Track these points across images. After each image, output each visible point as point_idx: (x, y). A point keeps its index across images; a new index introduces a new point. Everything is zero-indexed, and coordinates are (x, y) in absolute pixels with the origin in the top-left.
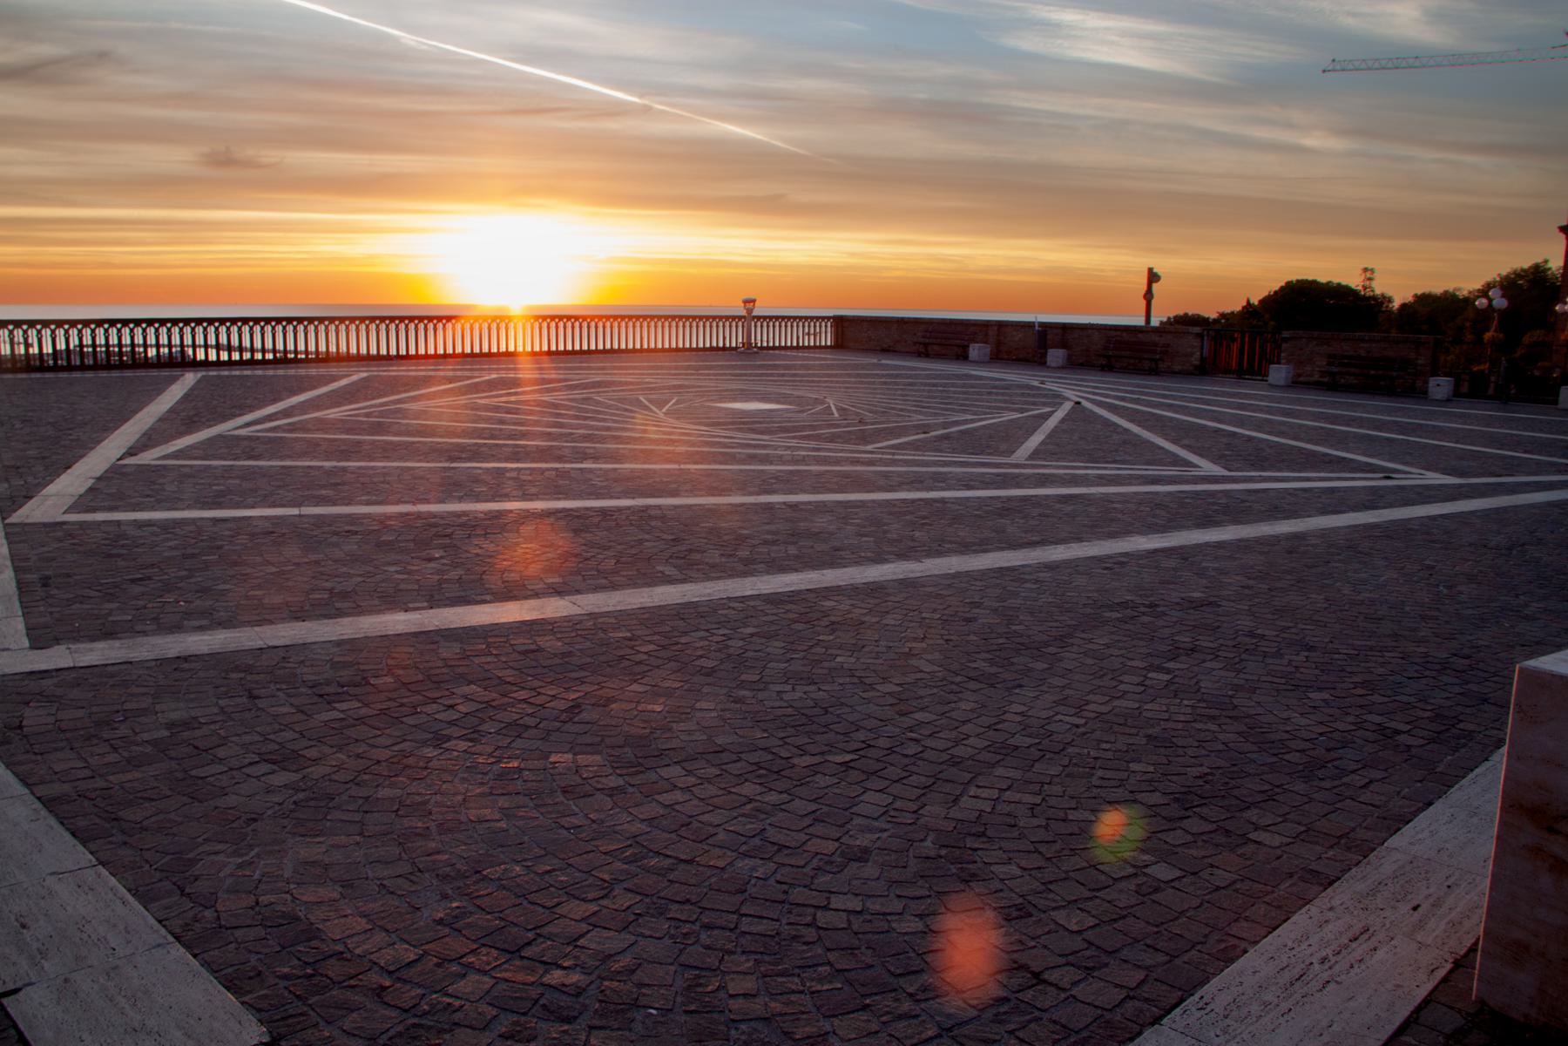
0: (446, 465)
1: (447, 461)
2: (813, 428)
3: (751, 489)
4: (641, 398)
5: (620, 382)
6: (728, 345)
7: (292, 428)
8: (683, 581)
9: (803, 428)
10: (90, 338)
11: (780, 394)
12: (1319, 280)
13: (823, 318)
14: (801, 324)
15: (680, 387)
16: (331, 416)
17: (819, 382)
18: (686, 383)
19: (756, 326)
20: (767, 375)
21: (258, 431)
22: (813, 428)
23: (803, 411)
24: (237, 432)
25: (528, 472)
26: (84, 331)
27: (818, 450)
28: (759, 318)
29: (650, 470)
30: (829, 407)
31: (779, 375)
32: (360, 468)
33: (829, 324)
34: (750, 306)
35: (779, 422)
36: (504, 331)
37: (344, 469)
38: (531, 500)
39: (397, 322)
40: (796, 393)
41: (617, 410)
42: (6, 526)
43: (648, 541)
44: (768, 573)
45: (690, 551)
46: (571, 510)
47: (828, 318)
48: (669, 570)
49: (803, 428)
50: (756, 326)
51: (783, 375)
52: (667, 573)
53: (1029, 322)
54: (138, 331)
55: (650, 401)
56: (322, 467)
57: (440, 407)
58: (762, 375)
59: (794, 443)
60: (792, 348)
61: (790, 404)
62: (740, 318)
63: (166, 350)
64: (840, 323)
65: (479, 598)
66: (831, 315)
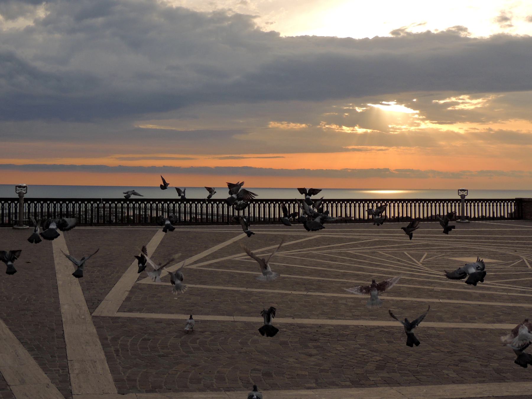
0: (305, 293)
1: (305, 291)
2: (517, 276)
3: (488, 319)
4: (406, 253)
5: (390, 241)
6: (421, 217)
7: (219, 265)
8: (461, 382)
9: (511, 277)
10: (14, 209)
11: (490, 252)
12: (275, 31)
13: (509, 200)
14: (453, 204)
15: (427, 245)
16: (237, 259)
17: (512, 243)
18: (430, 243)
19: (467, 206)
20: (478, 238)
21: (201, 266)
22: (517, 276)
23: (508, 264)
24: (194, 267)
25: (352, 300)
26: (44, 204)
27: (524, 292)
28: (468, 200)
29: (422, 302)
30: (524, 261)
31: (486, 238)
32: (260, 293)
33: (513, 204)
34: (464, 193)
35: (495, 272)
36: (393, 207)
37: (251, 293)
38: (357, 319)
39: (191, 202)
40: (501, 251)
41: (393, 260)
42: (94, 317)
43: (433, 352)
44: (514, 380)
45: (461, 361)
46: (383, 327)
47: (512, 200)
48: (453, 375)
49: (511, 277)
50: (467, 206)
51: (489, 238)
52: (451, 375)
53: (209, 195)
54: (52, 205)
55: (411, 255)
56: (239, 291)
57: (293, 255)
58: (475, 238)
59: (506, 287)
60: (497, 219)
61: (497, 259)
62: (457, 200)
63: (205, 217)
64: (519, 202)
65: (343, 383)
66: (514, 198)
